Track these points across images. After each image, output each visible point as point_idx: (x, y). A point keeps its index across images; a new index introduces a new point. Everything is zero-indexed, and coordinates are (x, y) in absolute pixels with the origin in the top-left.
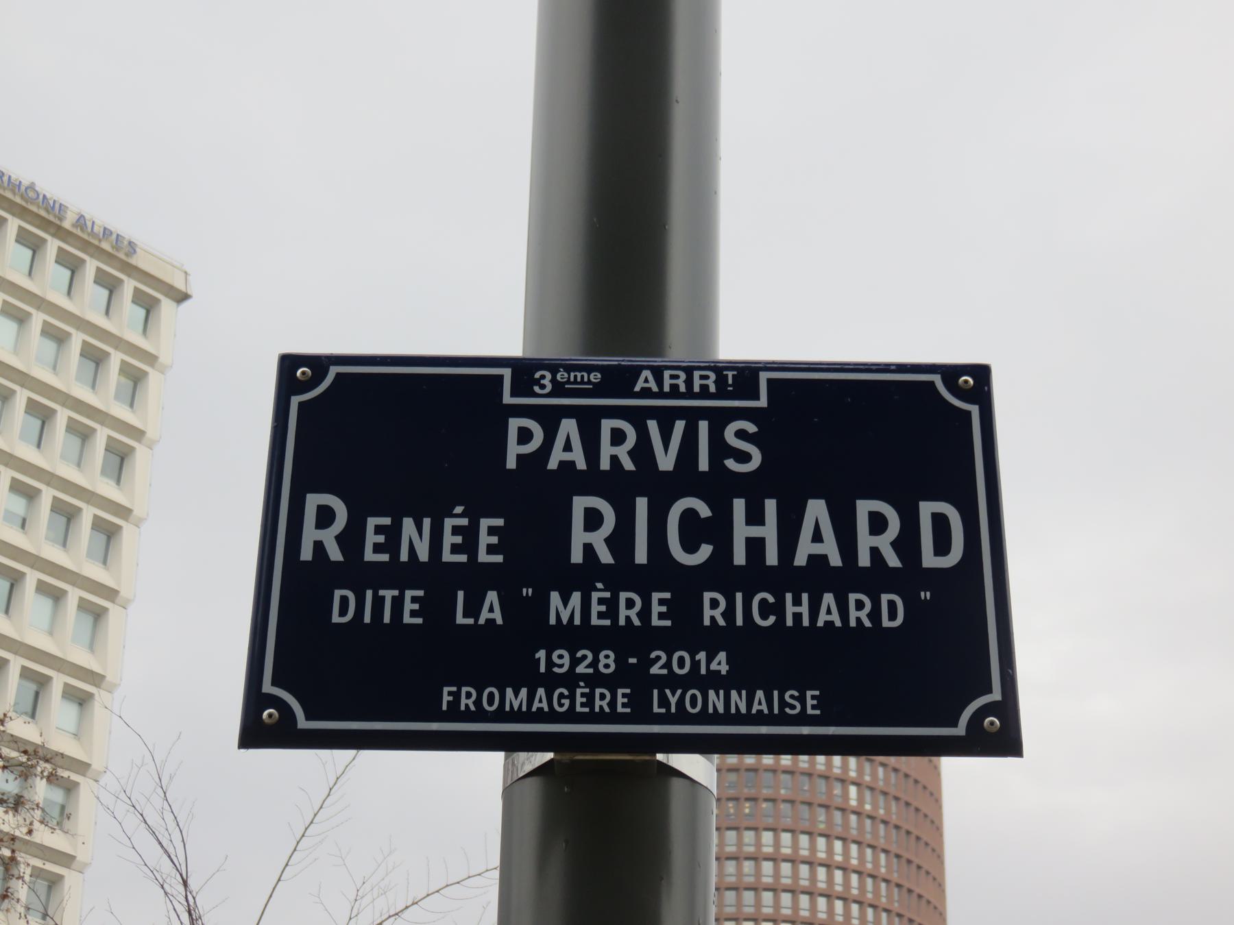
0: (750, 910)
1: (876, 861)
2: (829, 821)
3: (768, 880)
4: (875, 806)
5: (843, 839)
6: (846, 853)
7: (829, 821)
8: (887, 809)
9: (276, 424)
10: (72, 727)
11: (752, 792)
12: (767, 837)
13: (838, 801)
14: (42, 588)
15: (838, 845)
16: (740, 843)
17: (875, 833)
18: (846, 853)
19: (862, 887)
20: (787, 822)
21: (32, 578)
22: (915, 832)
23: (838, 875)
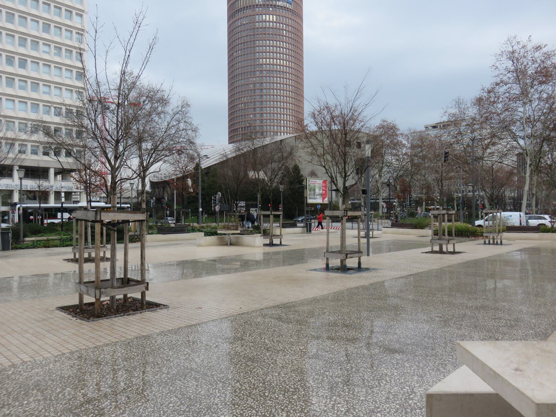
0: (265, 57)
1: (289, 46)
2: (280, 38)
3: (268, 57)
4: (289, 35)
5: (282, 42)
6: (283, 44)
7: (280, 38)
8: (291, 35)
9: (132, 312)
10: (70, 97)
11: (265, 33)
12: (268, 42)
13: (282, 34)
14: (77, 14)
15: (281, 25)
16: (262, 43)
17: (289, 40)
18: (283, 44)
19: (286, 69)
20: (272, 39)
21: (74, 12)
22: (298, 99)
23: (282, 55)
